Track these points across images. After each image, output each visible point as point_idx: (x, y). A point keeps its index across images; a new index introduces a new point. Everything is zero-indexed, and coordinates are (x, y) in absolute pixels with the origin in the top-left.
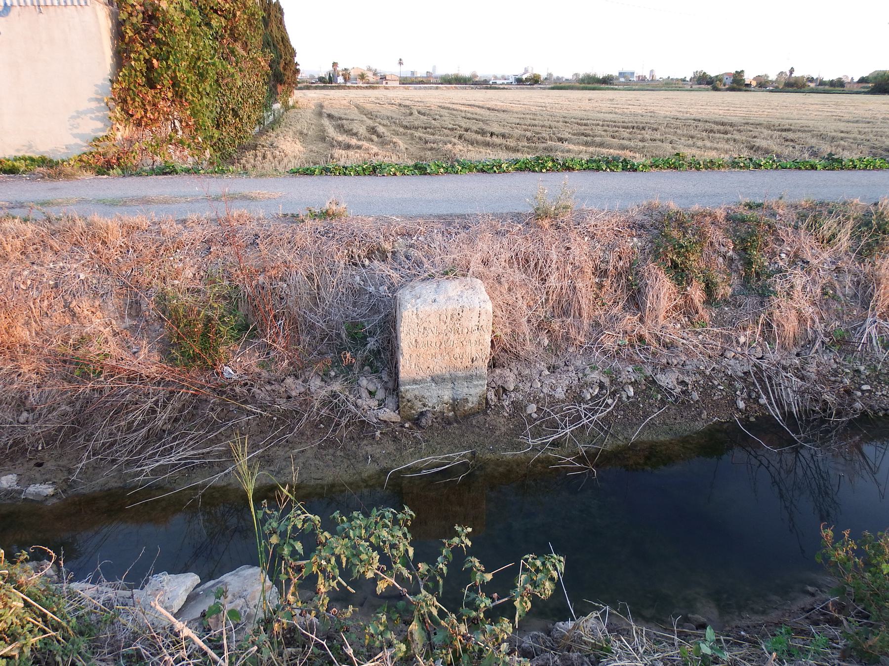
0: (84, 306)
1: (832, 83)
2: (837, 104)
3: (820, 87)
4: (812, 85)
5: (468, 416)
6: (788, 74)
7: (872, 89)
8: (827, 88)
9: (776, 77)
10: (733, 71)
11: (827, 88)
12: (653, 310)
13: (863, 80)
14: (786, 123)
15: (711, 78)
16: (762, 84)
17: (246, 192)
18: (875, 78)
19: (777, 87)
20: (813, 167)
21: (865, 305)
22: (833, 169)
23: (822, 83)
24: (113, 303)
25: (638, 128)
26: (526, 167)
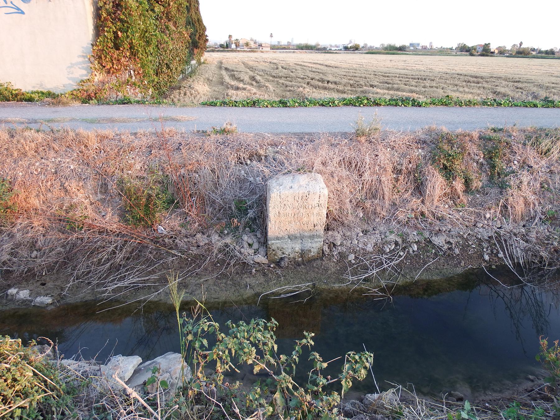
0: (72, 185)
1: (547, 52)
2: (550, 65)
4: (534, 53)
5: (311, 261)
6: (519, 46)
8: (543, 55)
9: (511, 48)
10: (483, 44)
11: (543, 55)
14: (517, 77)
15: (469, 48)
16: (502, 52)
19: (511, 54)
22: (548, 107)
23: (540, 52)
24: (90, 184)
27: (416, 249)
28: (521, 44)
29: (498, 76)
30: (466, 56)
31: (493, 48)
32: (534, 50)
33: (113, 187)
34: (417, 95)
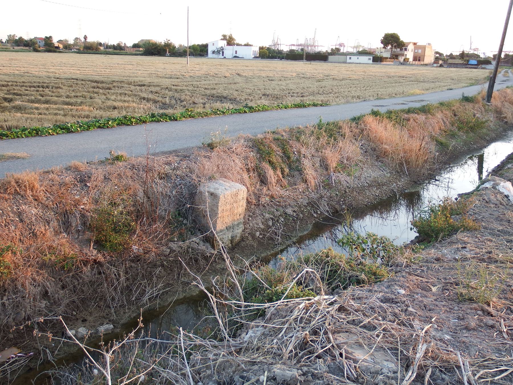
0: (40, 228)
1: (114, 47)
2: (138, 64)
3: (107, 50)
4: (102, 48)
5: (238, 244)
6: (83, 40)
7: (145, 52)
8: (111, 50)
9: (73, 42)
10: (44, 37)
11: (111, 50)
12: (270, 183)
13: (135, 46)
14: (97, 78)
15: (26, 41)
16: (67, 48)
17: (9, 153)
18: (144, 45)
19: (79, 49)
20: (245, 112)
21: (327, 169)
22: (252, 112)
23: (108, 47)
24: (54, 223)
25: (43, 87)
26: (122, 123)
27: (283, 220)
28: (85, 38)
29: (120, 80)
30: (30, 51)
31: (55, 41)
32: (100, 44)
33: (76, 222)
34: (75, 107)
